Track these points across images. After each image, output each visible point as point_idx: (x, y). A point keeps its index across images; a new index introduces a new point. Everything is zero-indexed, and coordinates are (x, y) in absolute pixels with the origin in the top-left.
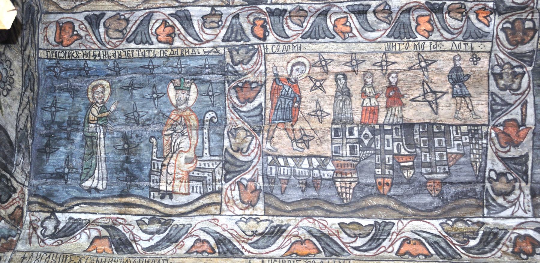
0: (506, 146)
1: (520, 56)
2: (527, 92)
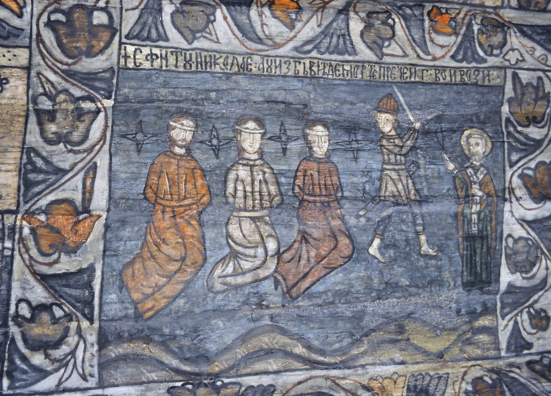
0: (51, 251)
1: (86, 79)
2: (97, 147)
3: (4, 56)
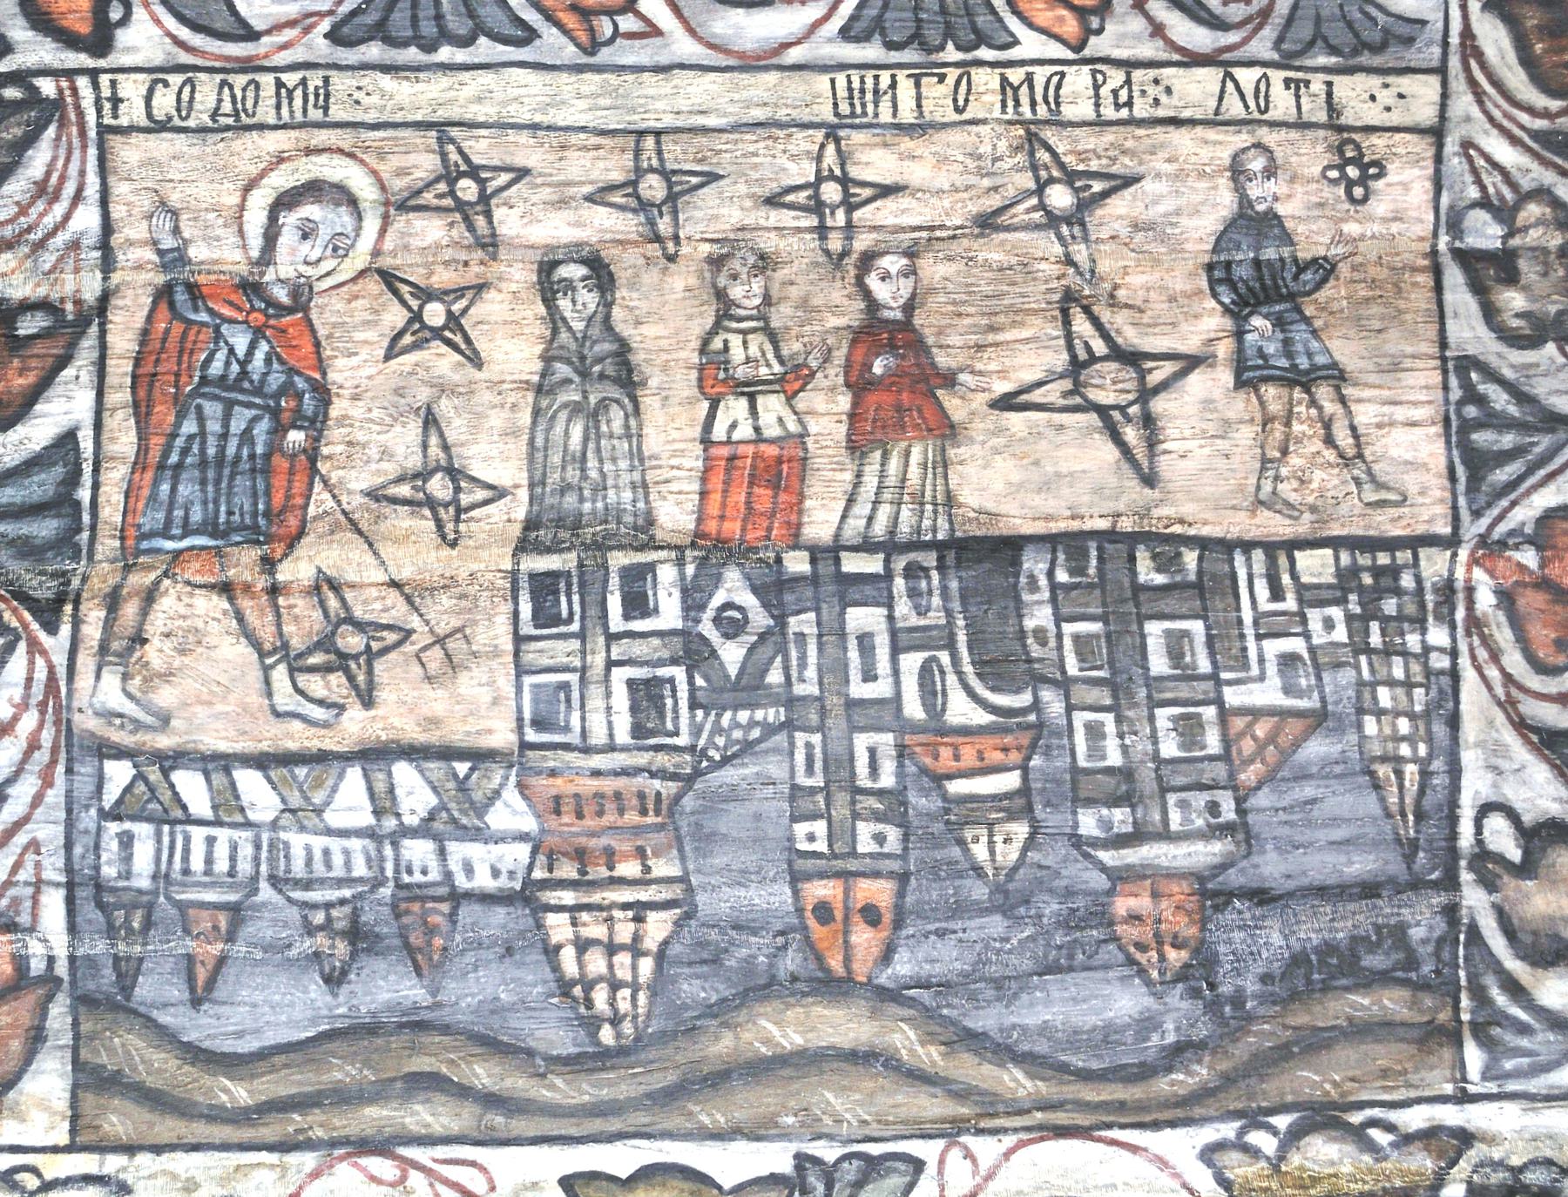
3: (1373, 98)
